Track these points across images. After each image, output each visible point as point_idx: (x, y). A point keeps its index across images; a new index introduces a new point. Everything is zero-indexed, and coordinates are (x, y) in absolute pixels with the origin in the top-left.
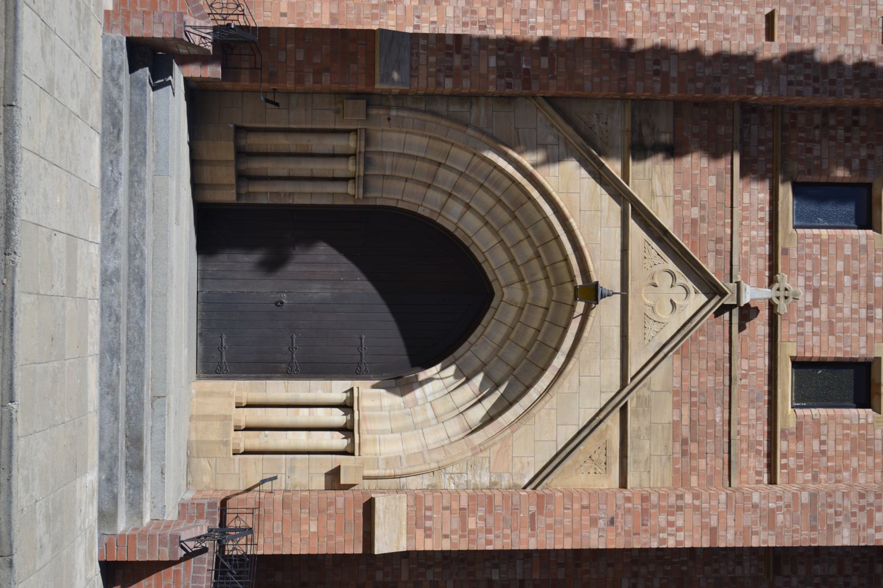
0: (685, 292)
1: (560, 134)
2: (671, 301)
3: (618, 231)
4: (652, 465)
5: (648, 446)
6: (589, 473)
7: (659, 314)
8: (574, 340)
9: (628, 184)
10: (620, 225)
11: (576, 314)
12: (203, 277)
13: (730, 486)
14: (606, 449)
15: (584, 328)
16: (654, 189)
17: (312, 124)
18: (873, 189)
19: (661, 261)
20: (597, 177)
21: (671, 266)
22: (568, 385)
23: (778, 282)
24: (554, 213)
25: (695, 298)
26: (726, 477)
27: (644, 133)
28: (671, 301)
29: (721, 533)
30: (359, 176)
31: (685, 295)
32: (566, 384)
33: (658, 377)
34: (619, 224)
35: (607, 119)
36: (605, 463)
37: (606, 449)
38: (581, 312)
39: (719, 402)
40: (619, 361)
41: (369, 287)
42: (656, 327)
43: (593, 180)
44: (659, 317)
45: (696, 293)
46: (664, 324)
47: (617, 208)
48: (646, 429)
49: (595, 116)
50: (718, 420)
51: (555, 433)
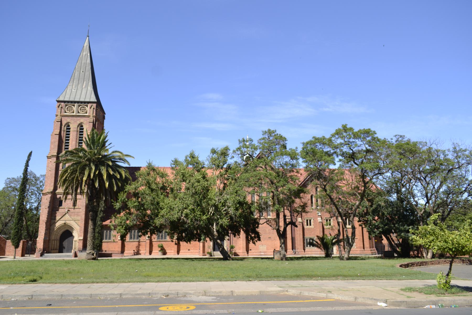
12: (65, 253)
32: (73, 224)
33: (73, 218)
41: (66, 240)
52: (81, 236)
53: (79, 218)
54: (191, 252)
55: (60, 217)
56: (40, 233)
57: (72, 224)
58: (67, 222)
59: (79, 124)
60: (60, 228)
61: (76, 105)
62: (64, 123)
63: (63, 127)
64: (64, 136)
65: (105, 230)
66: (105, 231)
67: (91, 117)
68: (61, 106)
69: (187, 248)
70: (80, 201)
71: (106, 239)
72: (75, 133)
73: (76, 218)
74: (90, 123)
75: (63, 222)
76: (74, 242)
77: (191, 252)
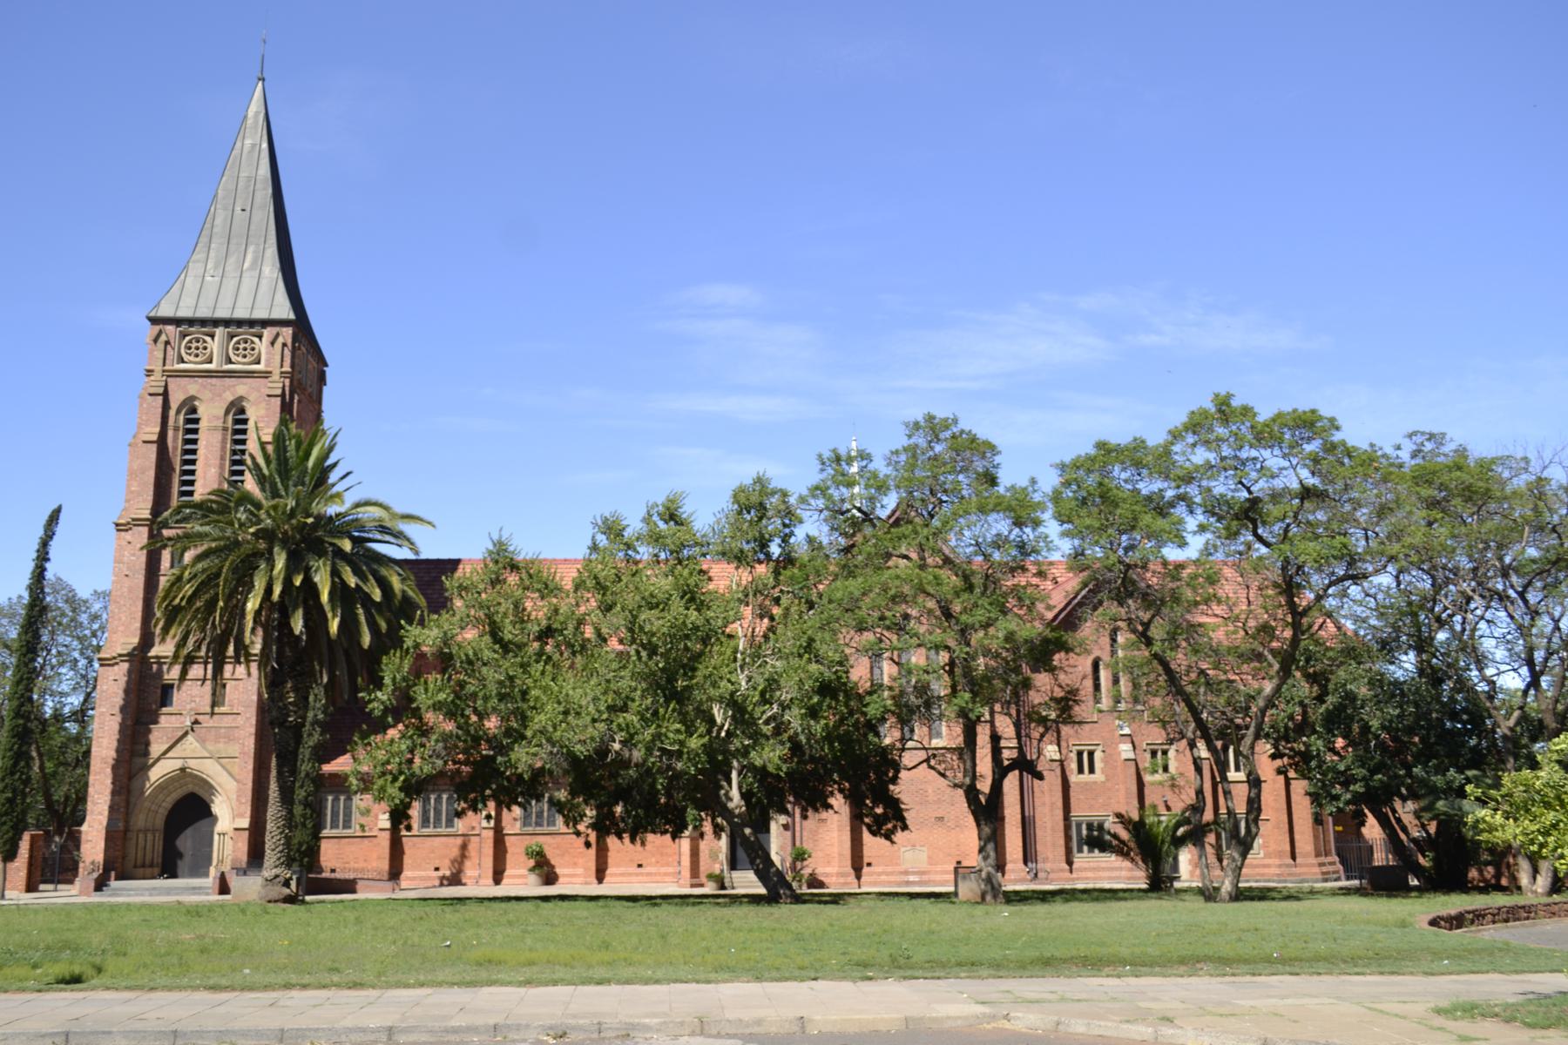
32: (210, 773)
52: (241, 815)
53: (234, 749)
54: (649, 874)
55: (166, 746)
56: (95, 804)
57: (211, 770)
58: (192, 763)
59: (232, 404)
60: (163, 787)
61: (220, 332)
62: (176, 399)
63: (172, 413)
64: (175, 448)
65: (331, 793)
66: (330, 798)
67: (276, 376)
68: (163, 338)
69: (632, 861)
70: (236, 688)
71: (334, 825)
72: (218, 436)
73: (222, 748)
74: (273, 399)
75: (178, 764)
76: (216, 837)
77: (649, 874)
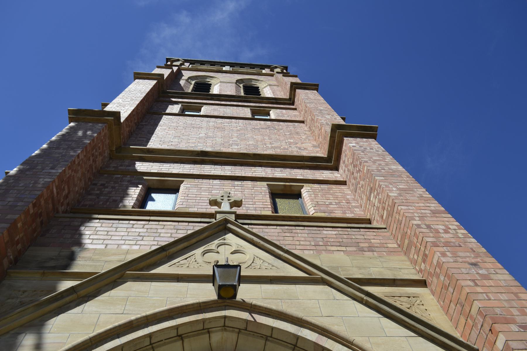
0: (224, 246)
1: (13, 332)
2: (232, 253)
3: (154, 284)
4: (393, 267)
5: (377, 269)
6: (426, 310)
7: (246, 260)
8: (281, 320)
9: (184, 91)
10: (150, 283)
11: (255, 316)
13: (385, 228)
14: (394, 297)
15: (266, 309)
16: (117, 260)
17: (467, 342)
18: (152, 187)
19: (193, 257)
20: (86, 299)
21: (198, 252)
22: (336, 326)
23: (217, 200)
24: (118, 338)
25: (229, 240)
26: (379, 230)
27: (54, 265)
28: (232, 253)
29: (433, 208)
30: (271, 146)
31: (226, 246)
34: (147, 284)
35: (19, 291)
36: (409, 297)
37: (394, 297)
38: (248, 314)
39: (319, 232)
40: (297, 286)
42: (257, 261)
43: (88, 303)
44: (249, 260)
45: (225, 240)
46: (256, 257)
47: (129, 285)
48: (360, 269)
49: (9, 301)
50: (335, 233)
51: (397, 338)
